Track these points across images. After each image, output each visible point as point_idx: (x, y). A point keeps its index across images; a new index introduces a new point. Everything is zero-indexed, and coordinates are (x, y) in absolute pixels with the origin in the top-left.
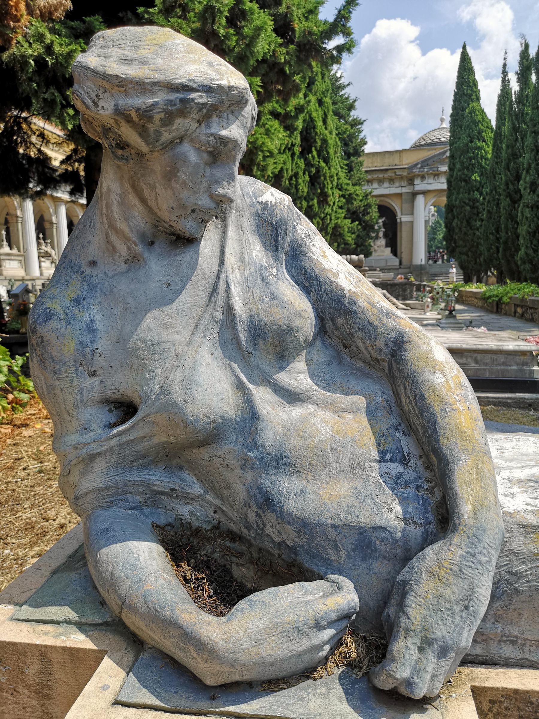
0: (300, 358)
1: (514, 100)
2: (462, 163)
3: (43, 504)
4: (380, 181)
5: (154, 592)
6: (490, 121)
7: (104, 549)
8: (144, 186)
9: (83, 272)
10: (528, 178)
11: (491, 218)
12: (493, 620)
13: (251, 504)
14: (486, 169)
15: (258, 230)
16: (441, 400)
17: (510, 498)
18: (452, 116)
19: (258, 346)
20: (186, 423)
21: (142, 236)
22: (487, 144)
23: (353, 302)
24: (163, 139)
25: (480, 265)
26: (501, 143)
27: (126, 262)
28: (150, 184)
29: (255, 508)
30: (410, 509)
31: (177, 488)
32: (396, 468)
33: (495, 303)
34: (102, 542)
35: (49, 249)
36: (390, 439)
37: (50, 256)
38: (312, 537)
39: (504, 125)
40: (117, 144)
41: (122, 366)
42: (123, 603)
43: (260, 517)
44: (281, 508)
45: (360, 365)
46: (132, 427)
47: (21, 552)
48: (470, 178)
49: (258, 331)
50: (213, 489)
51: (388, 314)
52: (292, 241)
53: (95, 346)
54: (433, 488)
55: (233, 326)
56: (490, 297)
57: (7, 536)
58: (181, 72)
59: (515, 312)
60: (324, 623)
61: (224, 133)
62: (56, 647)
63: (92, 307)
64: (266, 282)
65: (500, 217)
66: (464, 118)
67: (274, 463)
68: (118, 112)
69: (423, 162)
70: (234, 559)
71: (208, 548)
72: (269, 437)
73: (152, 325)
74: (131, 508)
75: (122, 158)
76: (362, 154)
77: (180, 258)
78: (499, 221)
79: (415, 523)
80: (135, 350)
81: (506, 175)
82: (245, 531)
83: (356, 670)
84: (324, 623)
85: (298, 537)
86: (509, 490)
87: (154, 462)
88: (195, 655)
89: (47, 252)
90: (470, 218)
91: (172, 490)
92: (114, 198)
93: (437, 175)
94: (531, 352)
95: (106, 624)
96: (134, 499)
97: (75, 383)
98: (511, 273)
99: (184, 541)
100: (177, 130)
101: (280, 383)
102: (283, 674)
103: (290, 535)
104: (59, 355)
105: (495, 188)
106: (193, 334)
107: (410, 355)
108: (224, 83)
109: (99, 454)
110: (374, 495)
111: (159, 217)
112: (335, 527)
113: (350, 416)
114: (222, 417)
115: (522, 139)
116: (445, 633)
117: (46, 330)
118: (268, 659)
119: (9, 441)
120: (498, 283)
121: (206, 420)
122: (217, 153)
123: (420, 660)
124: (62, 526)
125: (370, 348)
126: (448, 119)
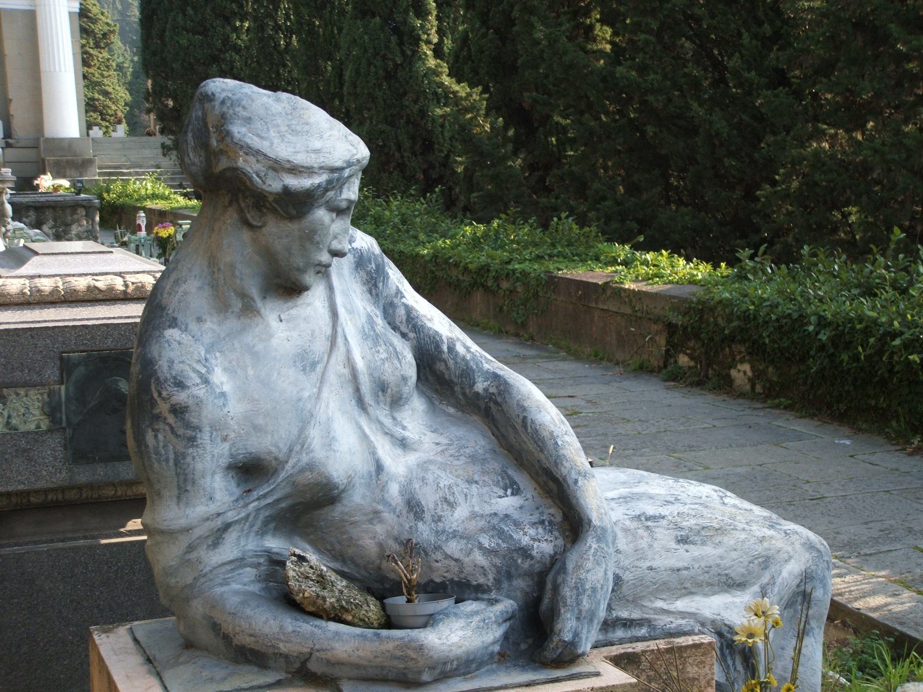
79: (546, 540)
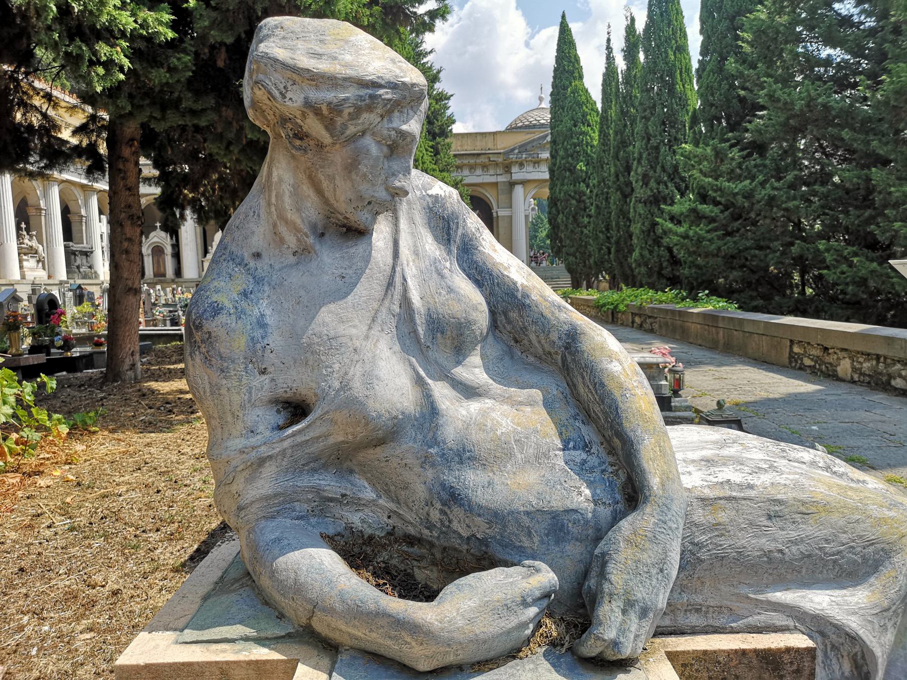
0: (476, 352)
1: (620, 80)
2: (566, 150)
3: (84, 568)
4: (472, 168)
5: (350, 590)
6: (595, 102)
7: (281, 558)
8: (322, 178)
9: (246, 265)
10: (640, 170)
11: (599, 213)
12: (679, 591)
13: (434, 502)
14: (592, 158)
15: (429, 223)
16: (621, 386)
17: (687, 476)
18: (551, 95)
19: (434, 340)
20: (367, 420)
21: (314, 227)
22: (592, 129)
23: (526, 296)
24: (348, 132)
25: (590, 268)
26: (607, 128)
27: (295, 254)
28: (329, 175)
29: (438, 505)
30: (598, 491)
31: (348, 493)
32: (579, 455)
33: (610, 311)
34: (276, 552)
35: (34, 243)
36: (570, 428)
37: (36, 253)
38: (505, 526)
39: (611, 108)
40: (295, 134)
41: (295, 362)
42: (315, 607)
43: (446, 514)
44: (469, 501)
45: (531, 359)
46: (307, 427)
47: (65, 627)
48: (575, 167)
49: (436, 325)
50: (387, 492)
51: (559, 307)
52: (463, 234)
53: (266, 342)
54: (617, 471)
55: (412, 320)
56: (604, 305)
57: (42, 609)
58: (370, 69)
59: (633, 322)
60: (529, 600)
61: (404, 127)
62: (240, 662)
63: (261, 301)
64: (442, 276)
65: (610, 213)
66: (566, 98)
67: (457, 459)
68: (308, 104)
69: (520, 147)
70: (415, 563)
71: (385, 555)
72: (450, 433)
73: (327, 320)
74: (298, 518)
75: (299, 148)
76: (449, 134)
77: (353, 250)
78: (609, 217)
79: (604, 503)
80: (309, 345)
81: (615, 165)
82: (426, 532)
83: (559, 648)
84: (529, 600)
85: (489, 528)
86: (686, 469)
87: (325, 467)
88: (409, 640)
89: (31, 247)
90: (576, 214)
91: (343, 495)
92: (286, 189)
93: (537, 162)
94: (658, 364)
95: (289, 636)
96: (301, 507)
97: (244, 381)
98: (624, 277)
99: (356, 550)
100: (363, 123)
101: (458, 378)
102: (492, 654)
103: (481, 528)
104: (228, 351)
105: (604, 181)
106: (370, 328)
107: (585, 345)
108: (407, 80)
109: (270, 457)
110: (563, 481)
111: (334, 209)
112: (527, 513)
113: (528, 409)
114: (403, 413)
115: (631, 124)
116: (644, 595)
117: (214, 325)
118: (482, 636)
119: (20, 494)
120: (610, 289)
121: (387, 415)
122: (396, 146)
123: (624, 622)
124: (115, 593)
125: (543, 342)
126: (548, 98)
